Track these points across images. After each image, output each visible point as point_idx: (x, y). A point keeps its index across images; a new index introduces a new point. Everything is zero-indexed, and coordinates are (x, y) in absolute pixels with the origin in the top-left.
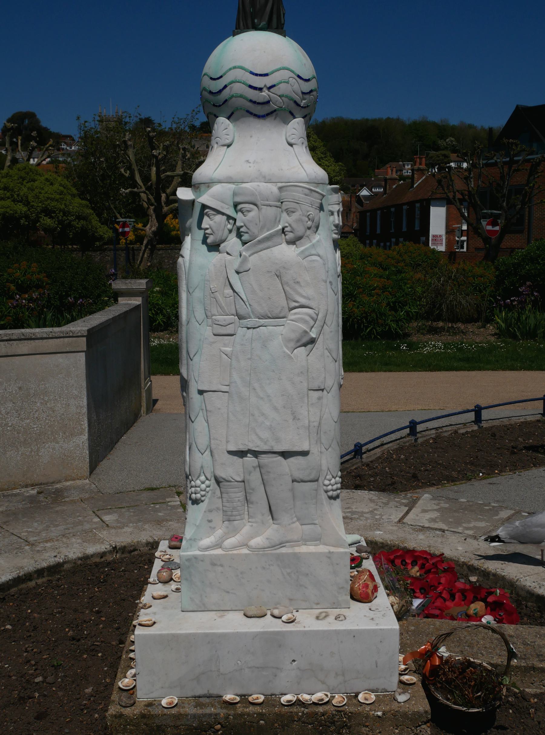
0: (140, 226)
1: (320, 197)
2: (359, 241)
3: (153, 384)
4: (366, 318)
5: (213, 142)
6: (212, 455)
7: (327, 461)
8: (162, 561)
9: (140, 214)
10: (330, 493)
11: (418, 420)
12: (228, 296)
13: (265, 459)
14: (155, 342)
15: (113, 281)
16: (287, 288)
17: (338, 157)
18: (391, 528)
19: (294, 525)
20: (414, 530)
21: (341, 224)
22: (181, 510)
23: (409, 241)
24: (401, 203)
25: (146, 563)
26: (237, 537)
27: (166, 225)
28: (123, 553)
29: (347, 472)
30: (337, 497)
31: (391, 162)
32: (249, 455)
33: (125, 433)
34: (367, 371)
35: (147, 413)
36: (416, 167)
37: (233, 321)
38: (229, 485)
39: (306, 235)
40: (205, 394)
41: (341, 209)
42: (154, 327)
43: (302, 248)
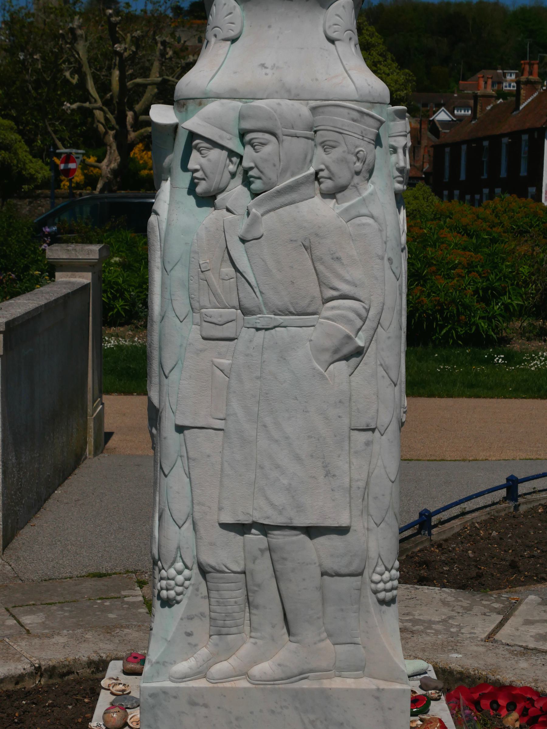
0: (92, 160)
1: (377, 124)
2: (433, 191)
3: (106, 408)
4: (441, 312)
5: (210, 34)
6: (194, 529)
7: (378, 543)
8: (112, 693)
9: (94, 143)
10: (381, 595)
11: (520, 476)
12: (227, 277)
13: (278, 538)
14: (111, 343)
15: (49, 245)
16: (320, 268)
17: (402, 60)
18: (475, 648)
19: (322, 645)
20: (512, 652)
21: (408, 167)
22: (144, 610)
23: (511, 193)
24: (499, 133)
25: (87, 694)
26: (231, 661)
27: (133, 160)
28: (51, 677)
29: (407, 556)
30: (393, 601)
31: (485, 69)
32: (253, 531)
33: (60, 485)
34: (440, 396)
35: (96, 454)
36: (523, 78)
37: (234, 318)
38: (221, 578)
39: (352, 184)
40: (186, 432)
41: (409, 144)
42: (109, 319)
43: (346, 205)
